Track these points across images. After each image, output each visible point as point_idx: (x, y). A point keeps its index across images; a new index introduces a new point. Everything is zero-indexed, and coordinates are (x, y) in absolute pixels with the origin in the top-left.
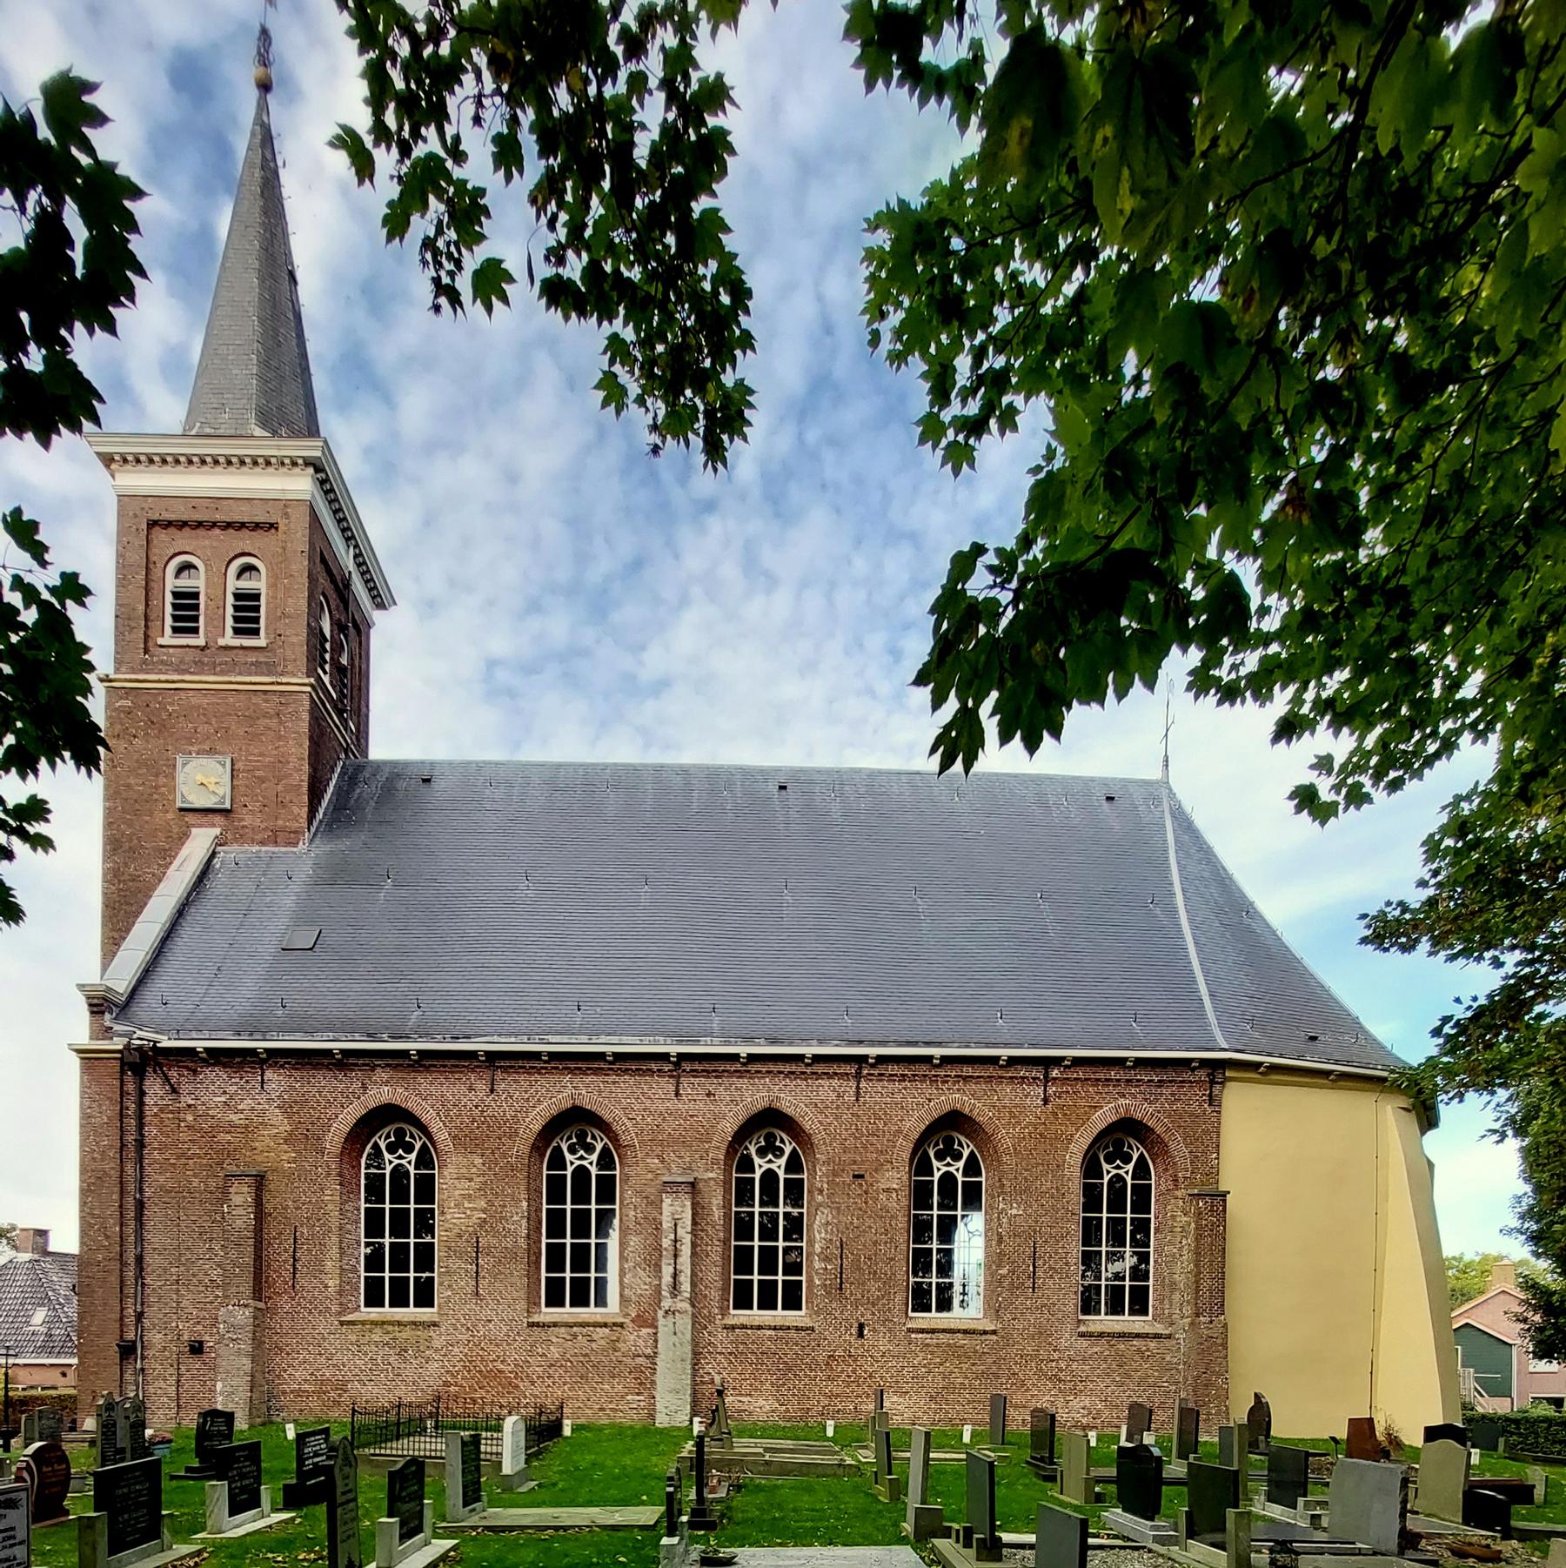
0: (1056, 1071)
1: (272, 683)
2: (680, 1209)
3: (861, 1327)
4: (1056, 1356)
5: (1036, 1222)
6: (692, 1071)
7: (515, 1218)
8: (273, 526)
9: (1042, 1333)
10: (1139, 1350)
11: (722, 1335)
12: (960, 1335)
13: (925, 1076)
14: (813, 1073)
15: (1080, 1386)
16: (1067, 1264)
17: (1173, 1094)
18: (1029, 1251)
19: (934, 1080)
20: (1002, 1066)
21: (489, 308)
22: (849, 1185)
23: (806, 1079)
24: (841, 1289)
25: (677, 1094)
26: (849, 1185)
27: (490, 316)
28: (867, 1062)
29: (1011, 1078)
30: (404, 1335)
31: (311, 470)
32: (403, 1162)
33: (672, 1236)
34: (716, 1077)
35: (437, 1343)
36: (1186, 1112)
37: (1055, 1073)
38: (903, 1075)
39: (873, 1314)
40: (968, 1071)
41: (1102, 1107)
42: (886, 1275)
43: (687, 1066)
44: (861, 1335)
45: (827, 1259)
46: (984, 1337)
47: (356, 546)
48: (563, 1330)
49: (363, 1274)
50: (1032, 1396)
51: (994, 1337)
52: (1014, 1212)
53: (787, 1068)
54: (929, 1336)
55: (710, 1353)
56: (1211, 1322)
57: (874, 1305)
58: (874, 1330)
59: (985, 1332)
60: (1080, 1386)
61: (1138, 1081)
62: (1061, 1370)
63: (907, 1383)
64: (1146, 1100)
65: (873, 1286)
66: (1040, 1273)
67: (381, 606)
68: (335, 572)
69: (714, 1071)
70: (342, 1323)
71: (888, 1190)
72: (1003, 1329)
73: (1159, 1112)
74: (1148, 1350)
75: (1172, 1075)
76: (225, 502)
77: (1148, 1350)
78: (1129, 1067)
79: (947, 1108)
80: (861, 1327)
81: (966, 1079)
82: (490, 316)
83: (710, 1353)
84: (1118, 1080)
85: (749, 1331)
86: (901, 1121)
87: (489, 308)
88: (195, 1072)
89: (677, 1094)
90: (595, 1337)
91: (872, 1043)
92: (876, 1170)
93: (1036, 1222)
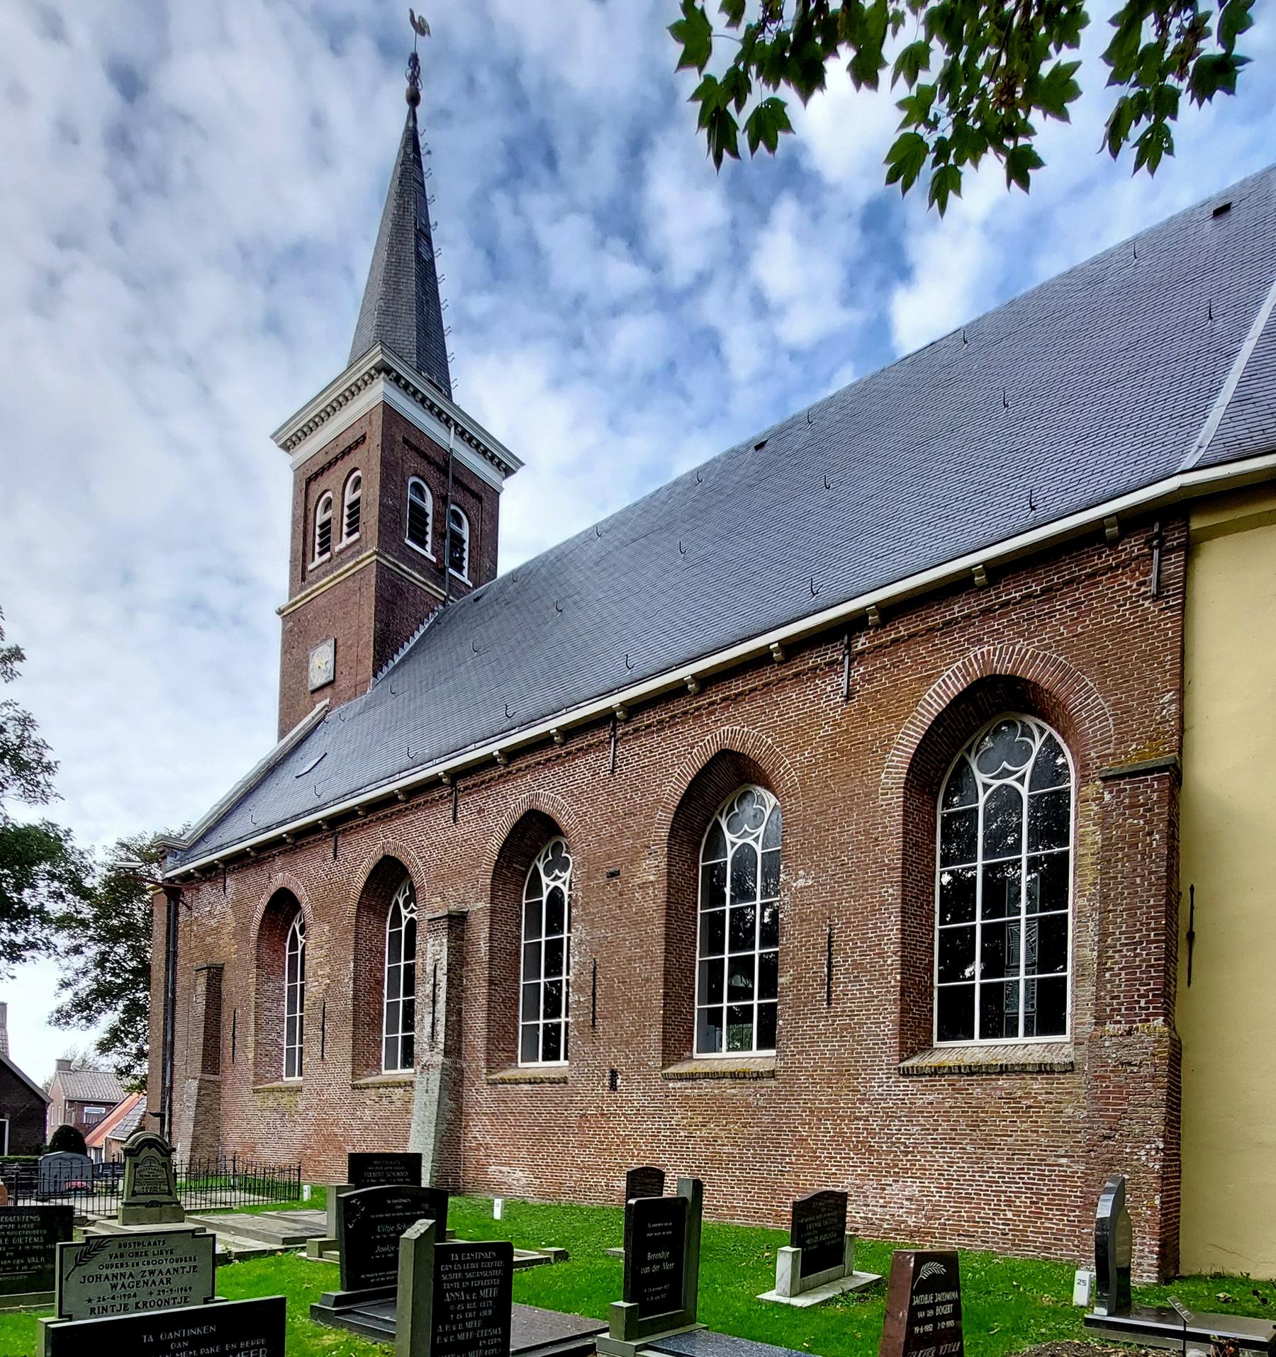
0: (862, 640)
1: (423, 583)
2: (439, 948)
3: (614, 1074)
4: (864, 1109)
5: (833, 893)
6: (466, 788)
7: (346, 981)
8: (364, 437)
9: (843, 1072)
10: (1010, 1098)
11: (486, 1091)
12: (727, 1082)
13: (685, 713)
14: (568, 754)
15: (904, 1162)
16: (880, 955)
17: (1075, 605)
18: (823, 942)
19: (696, 714)
20: (780, 663)
21: (1138, 166)
22: (604, 887)
23: (562, 764)
24: (594, 1026)
25: (455, 819)
26: (604, 887)
27: (1135, 171)
28: (616, 720)
29: (796, 675)
30: (284, 1101)
31: (383, 375)
32: (1009, 781)
33: (432, 982)
34: (486, 788)
35: (301, 1108)
36: (1103, 630)
37: (861, 643)
38: (660, 722)
39: (627, 1057)
40: (737, 686)
41: (940, 674)
42: (641, 1002)
43: (461, 785)
44: (613, 1087)
45: (580, 990)
46: (759, 1083)
47: (457, 425)
48: (373, 1091)
49: (285, 1047)
50: (829, 1176)
51: (773, 1083)
52: (801, 883)
53: (540, 757)
54: (689, 1084)
55: (477, 1113)
56: (1129, 1033)
57: (628, 1044)
58: (627, 1079)
59: (759, 1076)
60: (904, 1162)
61: (1007, 603)
62: (872, 1133)
63: (664, 1151)
64: (1021, 634)
65: (627, 1018)
66: (838, 975)
67: (508, 472)
68: (432, 454)
69: (483, 782)
70: (256, 1091)
71: (643, 886)
72: (786, 1069)
73: (1048, 648)
74: (1028, 1095)
75: (1071, 569)
76: (340, 438)
77: (1028, 1095)
78: (982, 588)
79: (714, 749)
80: (614, 1074)
81: (736, 699)
82: (1135, 171)
83: (477, 1113)
84: (968, 617)
85: (509, 1086)
86: (659, 786)
87: (1138, 166)
88: (198, 890)
89: (455, 819)
90: (395, 1098)
91: (610, 692)
92: (632, 862)
93: (833, 893)
